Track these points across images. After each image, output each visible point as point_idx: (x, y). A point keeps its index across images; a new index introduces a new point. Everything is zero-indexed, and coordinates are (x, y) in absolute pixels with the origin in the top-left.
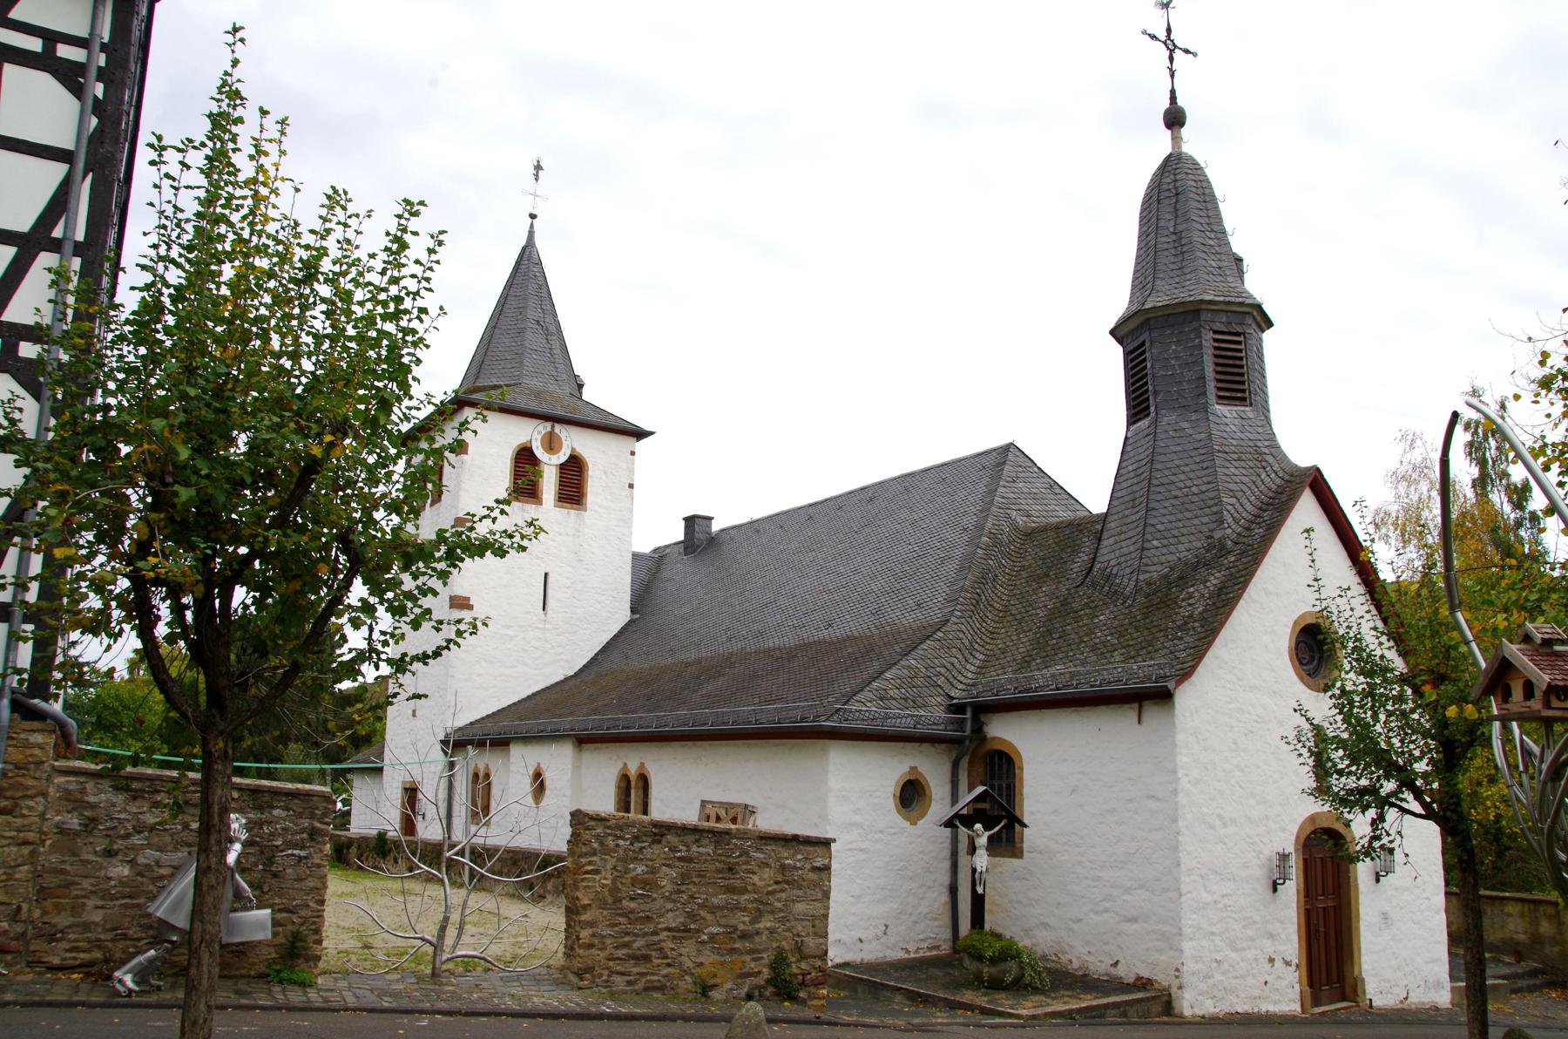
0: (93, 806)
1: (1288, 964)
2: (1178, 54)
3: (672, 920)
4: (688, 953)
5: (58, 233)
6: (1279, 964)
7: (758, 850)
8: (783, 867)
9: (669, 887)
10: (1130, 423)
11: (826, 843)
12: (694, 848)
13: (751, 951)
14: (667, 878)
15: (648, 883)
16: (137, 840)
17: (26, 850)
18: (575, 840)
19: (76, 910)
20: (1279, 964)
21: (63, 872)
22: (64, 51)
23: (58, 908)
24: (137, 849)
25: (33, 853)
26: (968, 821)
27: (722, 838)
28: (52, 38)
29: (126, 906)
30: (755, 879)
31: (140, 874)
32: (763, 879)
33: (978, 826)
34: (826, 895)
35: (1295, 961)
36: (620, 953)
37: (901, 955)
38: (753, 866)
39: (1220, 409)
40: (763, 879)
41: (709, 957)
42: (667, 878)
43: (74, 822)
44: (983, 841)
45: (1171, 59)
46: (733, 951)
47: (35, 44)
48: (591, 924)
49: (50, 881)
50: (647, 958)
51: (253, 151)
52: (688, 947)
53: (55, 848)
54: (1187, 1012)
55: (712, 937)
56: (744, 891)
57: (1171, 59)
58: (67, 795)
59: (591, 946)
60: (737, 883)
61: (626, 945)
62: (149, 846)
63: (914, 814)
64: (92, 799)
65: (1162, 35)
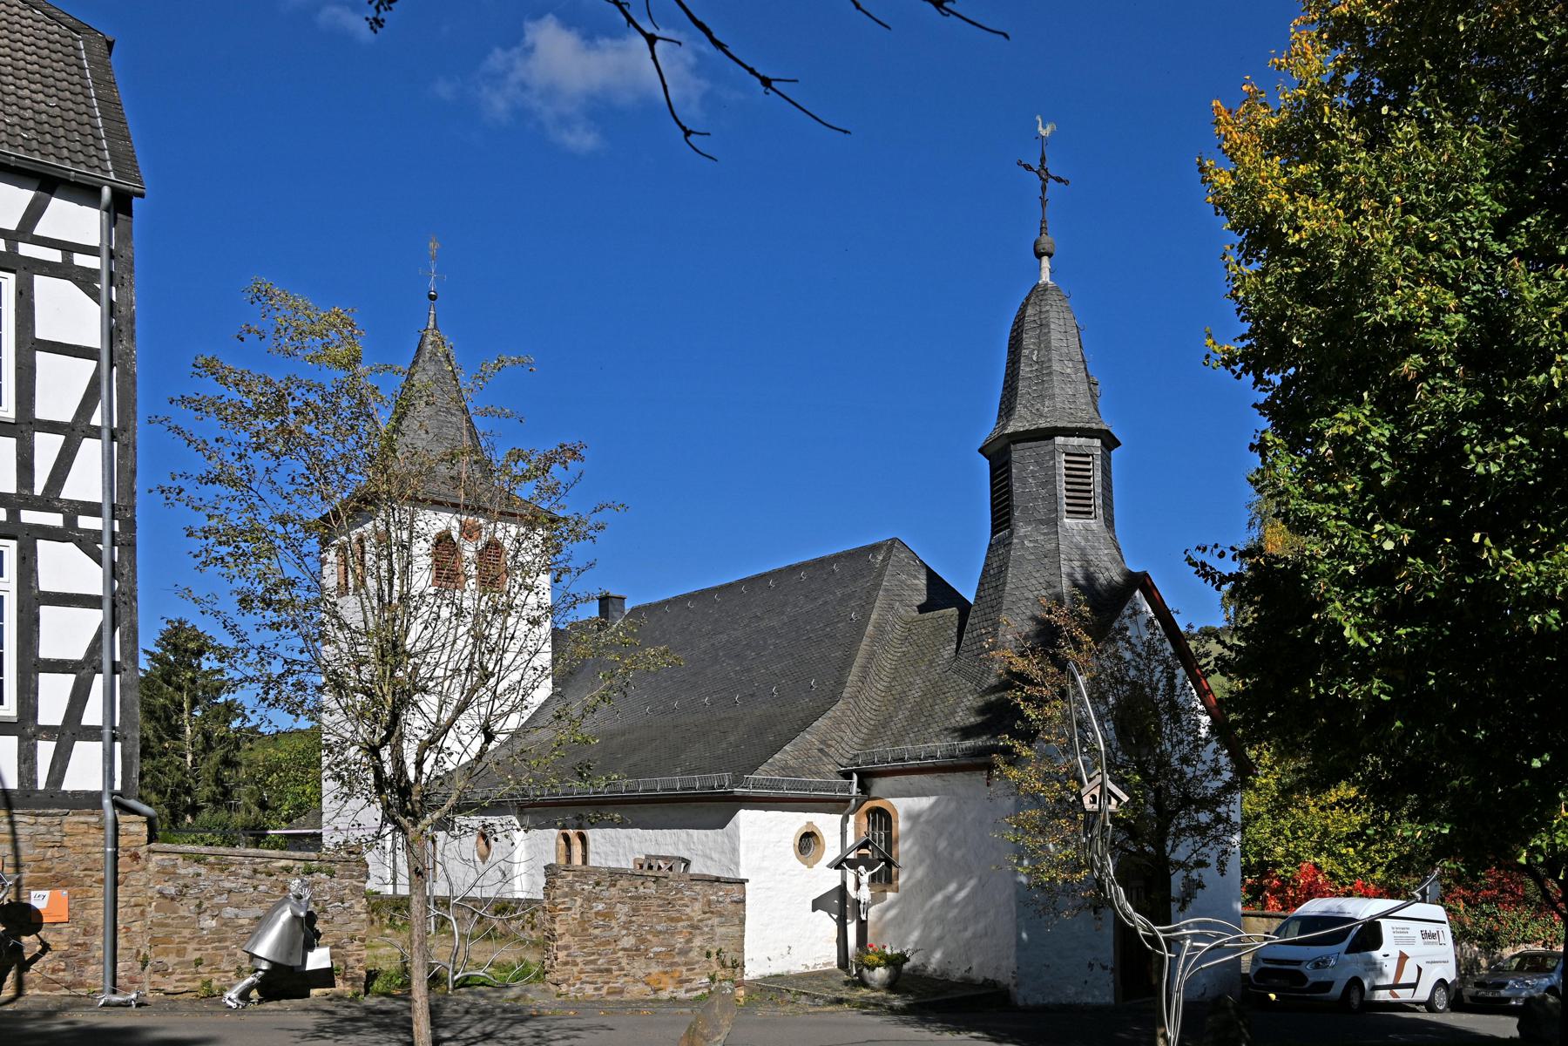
0: (184, 876)
1: (1105, 968)
2: (1051, 183)
3: (629, 942)
4: (639, 968)
5: (96, 420)
6: (1097, 968)
7: (690, 889)
8: (709, 903)
9: (623, 918)
10: (994, 533)
11: (742, 882)
12: (641, 889)
13: (685, 964)
14: (622, 911)
15: (608, 915)
16: (223, 899)
17: (137, 910)
18: (550, 885)
19: (180, 952)
20: (1097, 968)
21: (167, 925)
22: (80, 260)
23: (166, 952)
24: (220, 907)
25: (143, 913)
26: (853, 864)
27: (1193, 1013)
28: (68, 248)
29: (216, 948)
30: (688, 910)
31: (225, 924)
32: (695, 911)
33: (861, 868)
34: (742, 922)
35: (1110, 965)
36: (588, 968)
37: (802, 969)
38: (686, 900)
39: (1067, 521)
40: (695, 911)
41: (655, 970)
42: (622, 911)
43: (171, 890)
44: (865, 879)
45: (1044, 189)
46: (672, 964)
47: (55, 256)
48: (566, 947)
49: (160, 933)
50: (609, 971)
51: (197, 608)
52: (639, 963)
53: (158, 909)
54: (1020, 1003)
55: (657, 954)
56: (679, 920)
57: (1044, 189)
58: (163, 871)
59: (566, 963)
60: (674, 914)
61: (594, 962)
62: (229, 904)
63: (810, 860)
64: (182, 871)
65: (1036, 166)
